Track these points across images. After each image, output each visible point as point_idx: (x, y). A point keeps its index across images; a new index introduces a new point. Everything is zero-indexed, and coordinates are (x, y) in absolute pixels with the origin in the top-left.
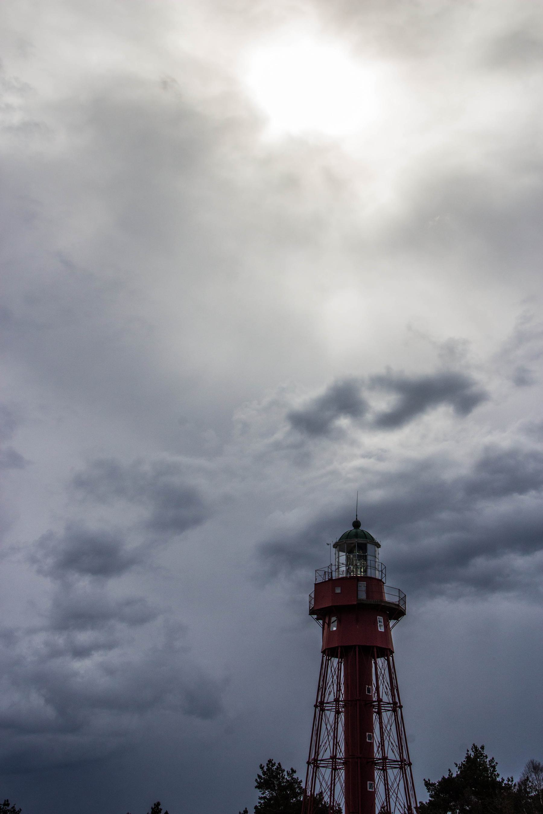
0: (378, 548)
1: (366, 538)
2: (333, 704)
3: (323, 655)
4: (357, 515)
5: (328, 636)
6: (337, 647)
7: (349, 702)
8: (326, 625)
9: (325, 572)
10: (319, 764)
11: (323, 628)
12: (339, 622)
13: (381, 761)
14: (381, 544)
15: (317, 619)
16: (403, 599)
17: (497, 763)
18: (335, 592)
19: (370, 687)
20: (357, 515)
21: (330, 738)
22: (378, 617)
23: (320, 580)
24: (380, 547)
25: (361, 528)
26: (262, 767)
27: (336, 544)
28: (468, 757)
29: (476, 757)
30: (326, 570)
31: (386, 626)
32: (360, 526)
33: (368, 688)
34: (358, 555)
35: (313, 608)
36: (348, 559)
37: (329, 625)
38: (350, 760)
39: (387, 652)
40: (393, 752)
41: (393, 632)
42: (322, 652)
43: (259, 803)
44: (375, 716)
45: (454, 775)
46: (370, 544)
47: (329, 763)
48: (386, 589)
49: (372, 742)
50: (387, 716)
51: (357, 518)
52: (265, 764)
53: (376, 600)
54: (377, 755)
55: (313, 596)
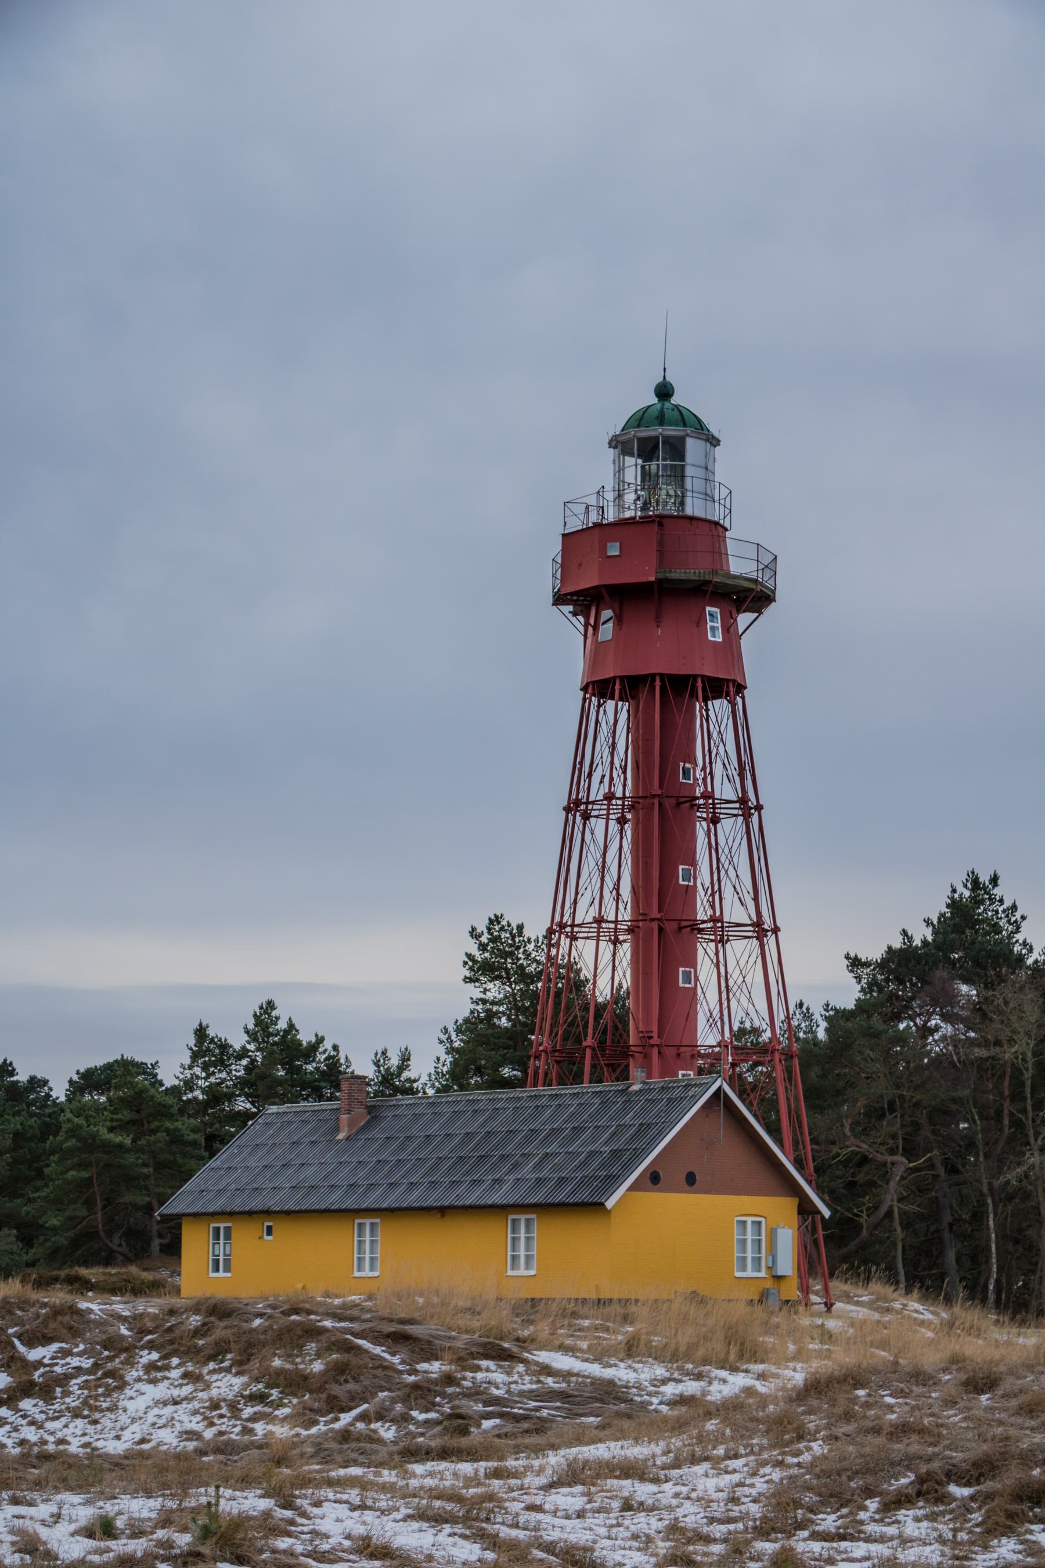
0: (715, 446)
1: (685, 425)
2: (602, 804)
3: (585, 696)
4: (665, 369)
5: (596, 654)
6: (614, 678)
8: (590, 630)
9: (587, 508)
10: (577, 932)
13: (710, 925)
14: (720, 439)
15: (575, 614)
16: (772, 567)
17: (1023, 918)
19: (688, 765)
20: (665, 369)
21: (727, 851)
22: (708, 609)
23: (575, 525)
24: (719, 445)
25: (675, 400)
26: (474, 933)
28: (954, 905)
29: (977, 902)
31: (729, 628)
32: (672, 395)
33: (684, 768)
34: (663, 464)
35: (559, 590)
36: (645, 474)
37: (596, 628)
38: (641, 924)
39: (728, 687)
40: (742, 905)
41: (746, 644)
42: (581, 690)
44: (701, 829)
45: (917, 942)
46: (692, 437)
47: (591, 930)
48: (731, 547)
49: (691, 884)
50: (730, 828)
52: (482, 927)
53: (702, 571)
54: (702, 912)
55: (559, 560)
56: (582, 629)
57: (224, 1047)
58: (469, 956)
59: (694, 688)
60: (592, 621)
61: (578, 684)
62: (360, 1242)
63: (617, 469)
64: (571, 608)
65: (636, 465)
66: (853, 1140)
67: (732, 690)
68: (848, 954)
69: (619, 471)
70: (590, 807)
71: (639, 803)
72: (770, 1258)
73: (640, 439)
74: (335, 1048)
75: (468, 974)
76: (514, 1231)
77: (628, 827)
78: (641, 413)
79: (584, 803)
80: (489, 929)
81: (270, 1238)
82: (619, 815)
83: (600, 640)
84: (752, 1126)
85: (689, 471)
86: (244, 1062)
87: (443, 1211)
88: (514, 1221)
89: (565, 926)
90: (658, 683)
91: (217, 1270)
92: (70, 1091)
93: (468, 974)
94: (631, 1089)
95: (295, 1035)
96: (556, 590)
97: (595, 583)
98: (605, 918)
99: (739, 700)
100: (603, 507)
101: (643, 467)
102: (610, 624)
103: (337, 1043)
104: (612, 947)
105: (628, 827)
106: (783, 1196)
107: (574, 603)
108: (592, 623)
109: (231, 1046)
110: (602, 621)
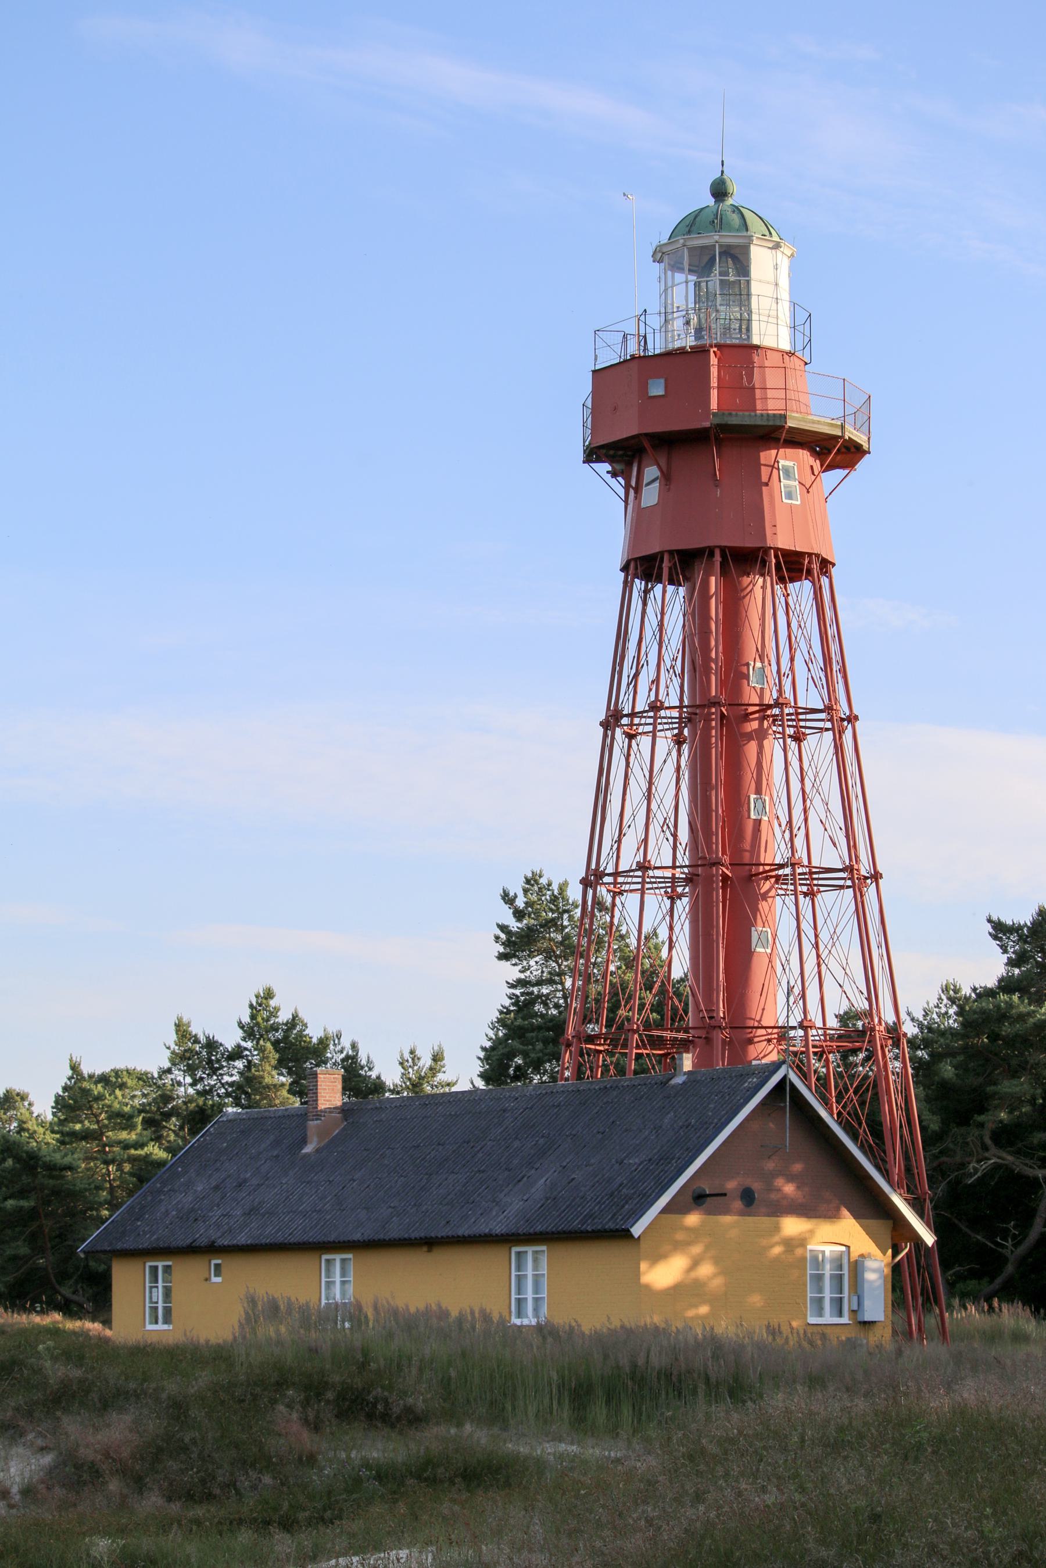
4: (722, 161)
6: (662, 553)
7: (698, 711)
9: (625, 337)
11: (626, 502)
12: (666, 477)
15: (614, 474)
18: (647, 393)
20: (722, 161)
23: (609, 358)
26: (508, 899)
27: (659, 251)
30: (631, 328)
37: (638, 490)
43: (511, 998)
51: (722, 172)
52: (516, 888)
55: (589, 404)
56: (622, 494)
57: (212, 1045)
58: (503, 928)
59: (764, 563)
60: (633, 484)
61: (618, 563)
62: (328, 1284)
63: (663, 288)
64: (607, 467)
65: (687, 282)
66: (993, 1150)
67: (815, 567)
68: (990, 916)
69: (666, 290)
70: (636, 721)
71: (696, 714)
72: (855, 1299)
73: (691, 250)
74: (354, 1046)
75: (502, 949)
76: (519, 1268)
77: (685, 748)
78: (692, 217)
79: (626, 716)
80: (526, 891)
81: (219, 1280)
82: (676, 731)
83: (643, 505)
84: (828, 1127)
85: (755, 288)
86: (240, 1064)
87: (430, 1243)
88: (519, 1254)
89: (603, 874)
90: (718, 558)
91: (156, 1323)
92: (58, 1109)
93: (502, 949)
94: (673, 1082)
95: (302, 1031)
96: (587, 443)
97: (634, 431)
98: (652, 863)
99: (825, 581)
100: (645, 337)
101: (697, 285)
102: (656, 484)
103: (356, 1040)
104: (668, 902)
105: (685, 748)
106: (872, 1218)
107: (611, 460)
108: (634, 485)
109: (221, 1045)
110: (645, 482)
